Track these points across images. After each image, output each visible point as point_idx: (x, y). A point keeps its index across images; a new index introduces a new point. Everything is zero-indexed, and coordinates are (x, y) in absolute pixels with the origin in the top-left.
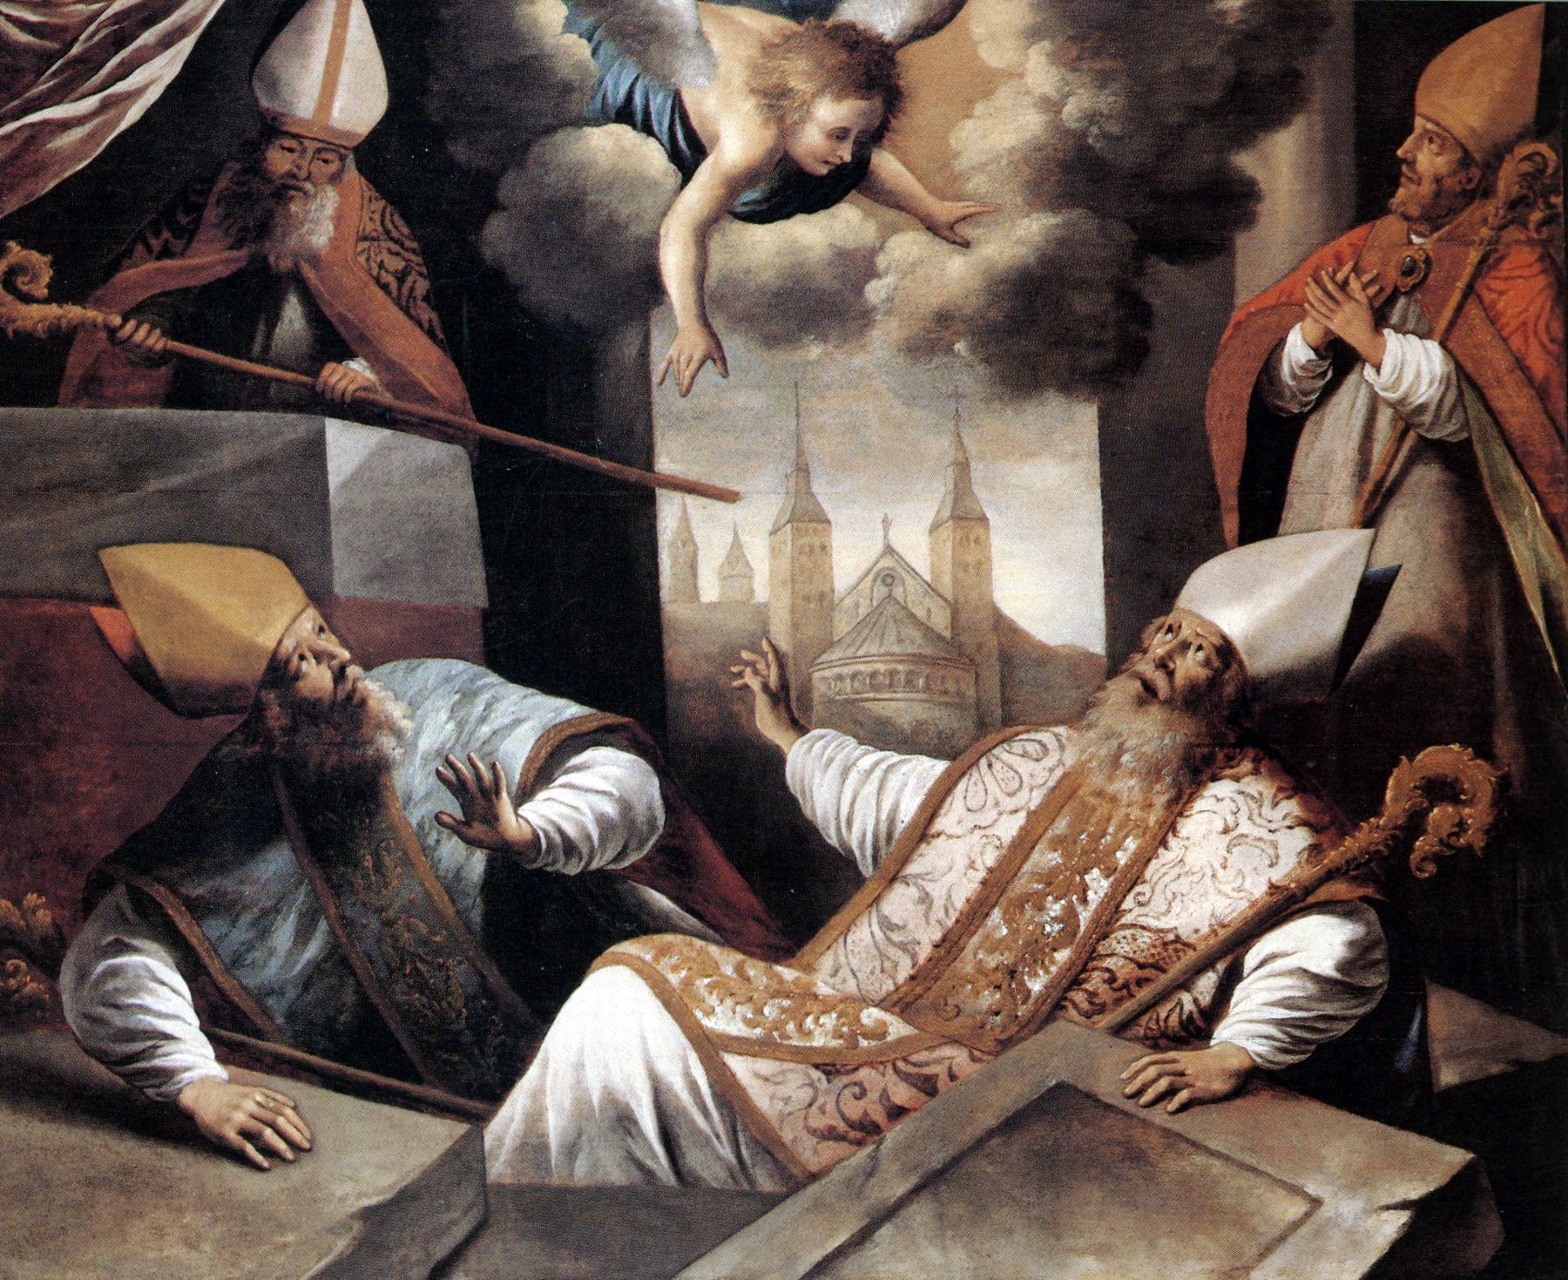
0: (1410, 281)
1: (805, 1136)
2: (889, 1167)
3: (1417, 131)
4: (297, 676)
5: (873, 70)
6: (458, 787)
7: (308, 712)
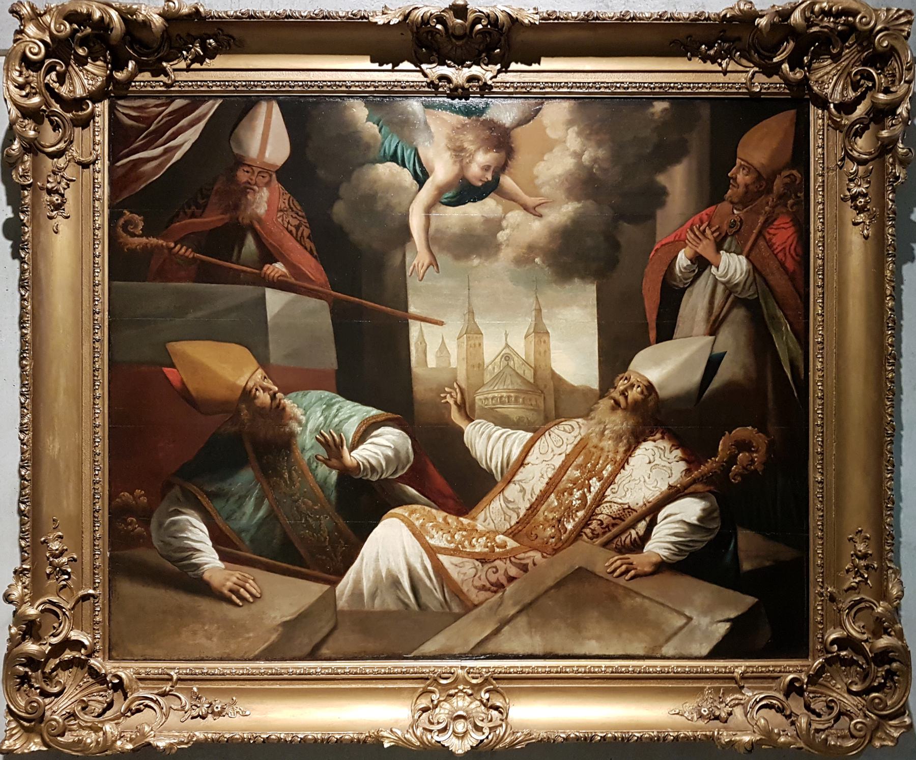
0: (734, 230)
1: (473, 589)
2: (508, 602)
3: (738, 165)
4: (255, 397)
5: (501, 140)
6: (325, 444)
7: (261, 412)
